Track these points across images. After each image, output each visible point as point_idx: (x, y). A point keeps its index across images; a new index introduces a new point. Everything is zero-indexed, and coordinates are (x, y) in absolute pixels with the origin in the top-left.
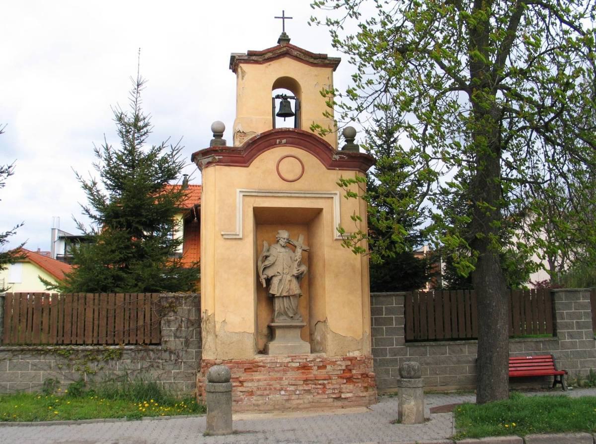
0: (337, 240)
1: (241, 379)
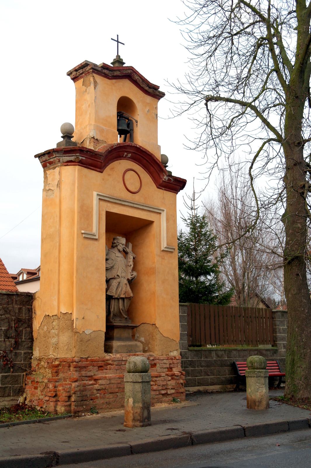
0: (163, 251)
1: (96, 377)
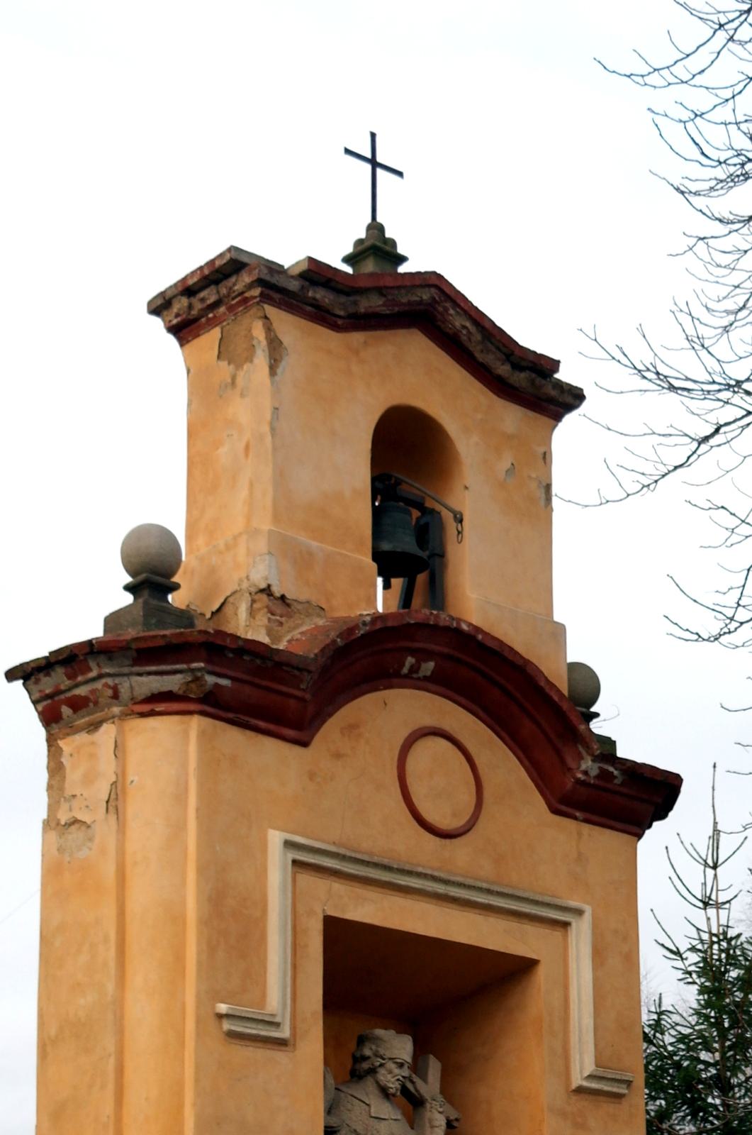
0: (580, 1090)
